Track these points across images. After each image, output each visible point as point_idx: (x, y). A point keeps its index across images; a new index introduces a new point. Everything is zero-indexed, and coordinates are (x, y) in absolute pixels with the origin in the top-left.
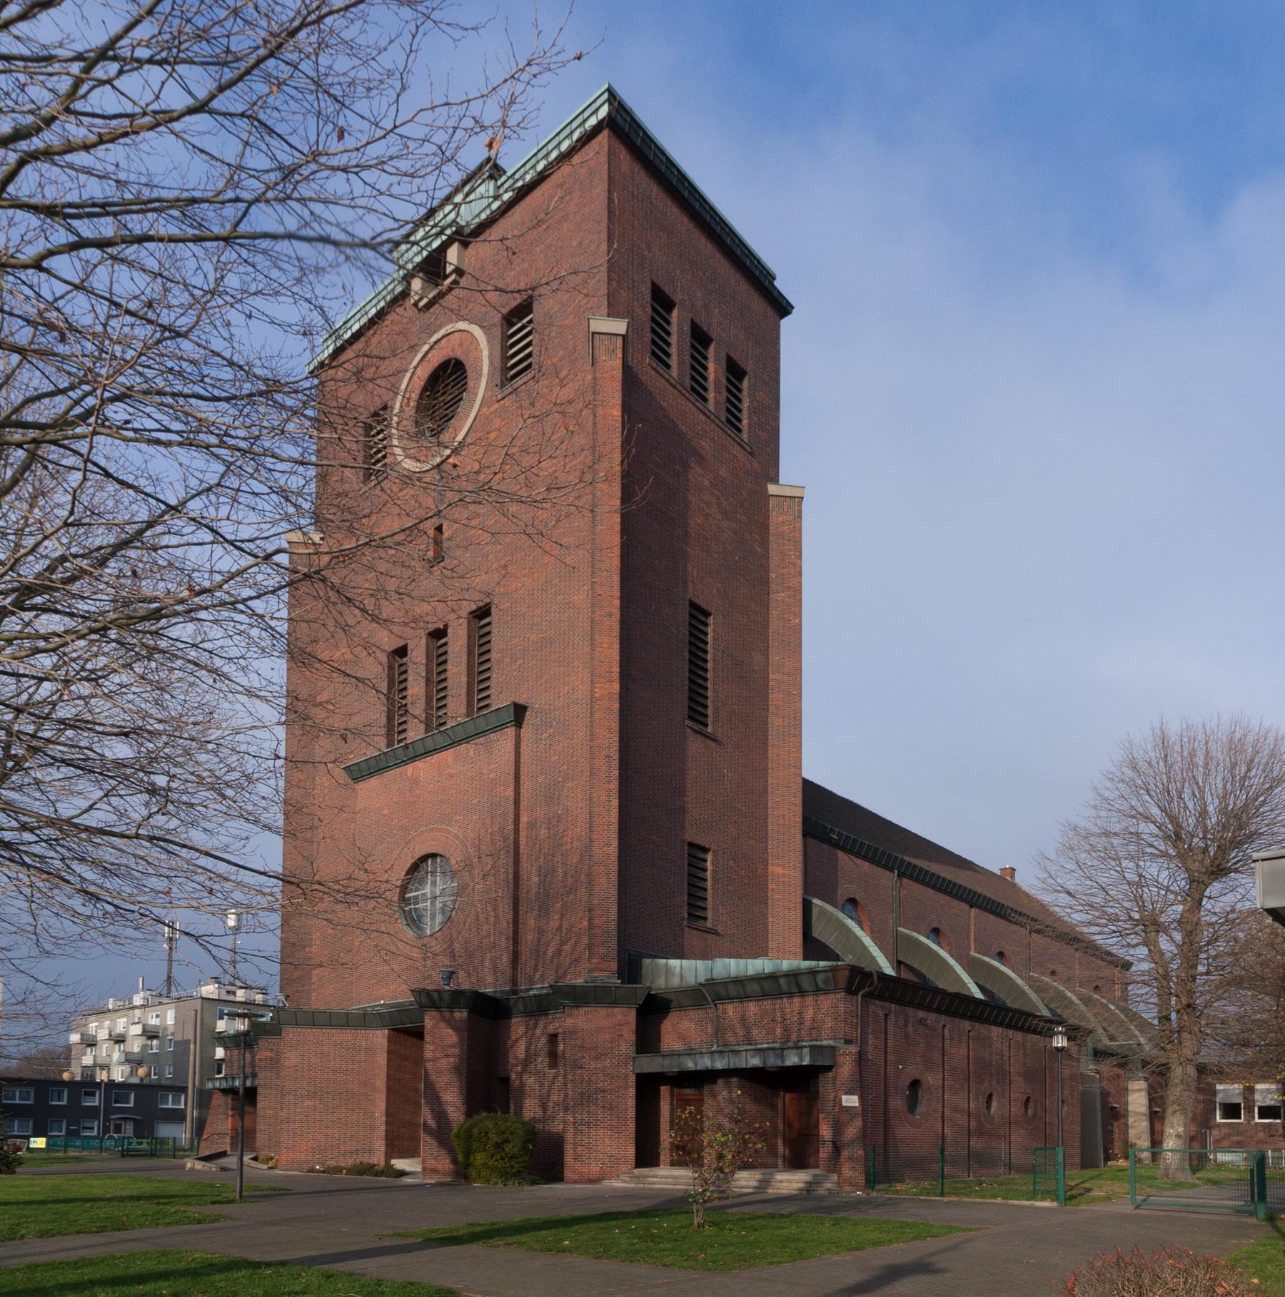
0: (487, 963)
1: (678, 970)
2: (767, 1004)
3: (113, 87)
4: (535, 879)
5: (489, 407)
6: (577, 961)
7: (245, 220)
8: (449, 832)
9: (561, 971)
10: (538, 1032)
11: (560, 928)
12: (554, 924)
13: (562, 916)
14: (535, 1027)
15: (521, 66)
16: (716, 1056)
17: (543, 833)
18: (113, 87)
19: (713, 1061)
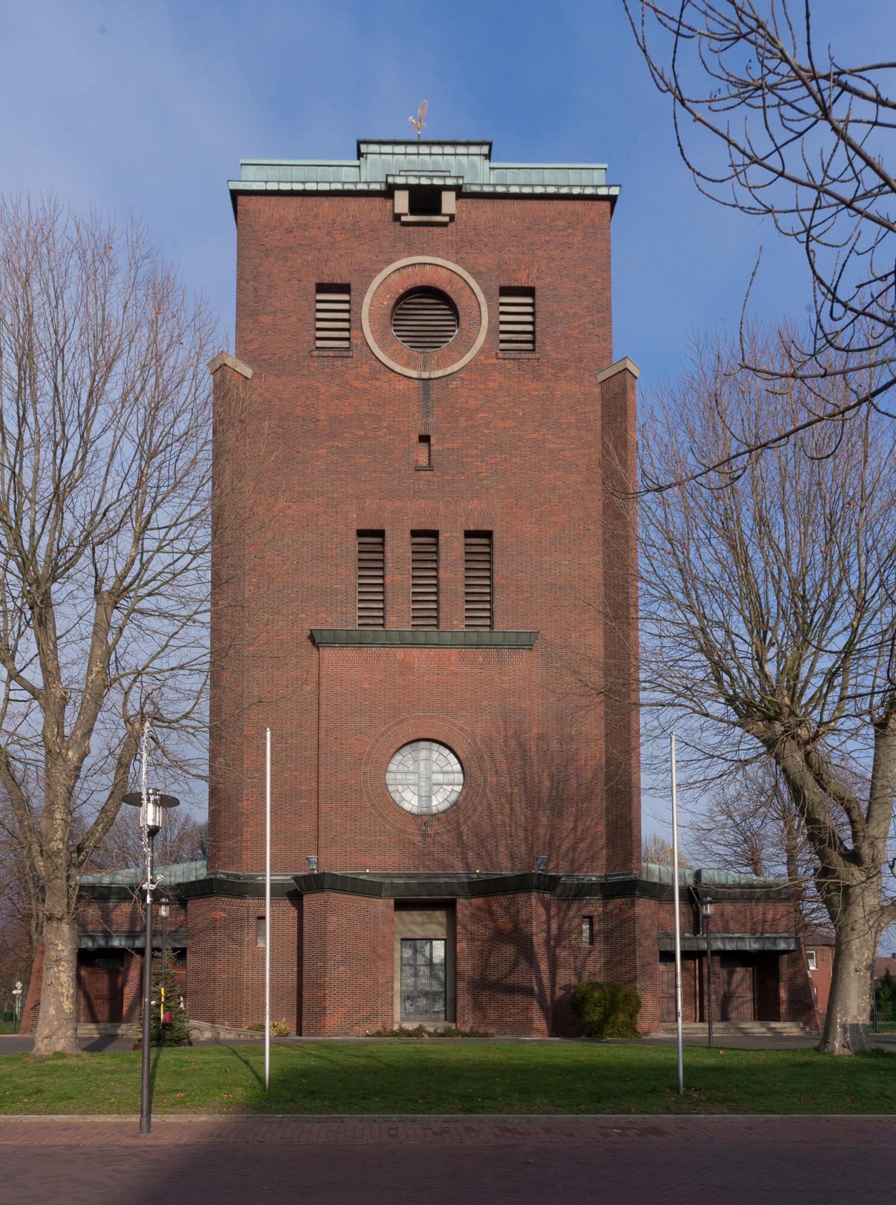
0: (502, 849)
1: (657, 873)
2: (739, 906)
3: (809, 210)
4: (547, 783)
5: (487, 358)
6: (593, 858)
7: (862, 364)
8: (454, 724)
9: (576, 865)
10: (572, 913)
11: (574, 829)
12: (568, 823)
13: (576, 820)
14: (568, 908)
15: (852, 304)
16: (726, 941)
17: (555, 746)
18: (809, 210)
19: (788, 944)
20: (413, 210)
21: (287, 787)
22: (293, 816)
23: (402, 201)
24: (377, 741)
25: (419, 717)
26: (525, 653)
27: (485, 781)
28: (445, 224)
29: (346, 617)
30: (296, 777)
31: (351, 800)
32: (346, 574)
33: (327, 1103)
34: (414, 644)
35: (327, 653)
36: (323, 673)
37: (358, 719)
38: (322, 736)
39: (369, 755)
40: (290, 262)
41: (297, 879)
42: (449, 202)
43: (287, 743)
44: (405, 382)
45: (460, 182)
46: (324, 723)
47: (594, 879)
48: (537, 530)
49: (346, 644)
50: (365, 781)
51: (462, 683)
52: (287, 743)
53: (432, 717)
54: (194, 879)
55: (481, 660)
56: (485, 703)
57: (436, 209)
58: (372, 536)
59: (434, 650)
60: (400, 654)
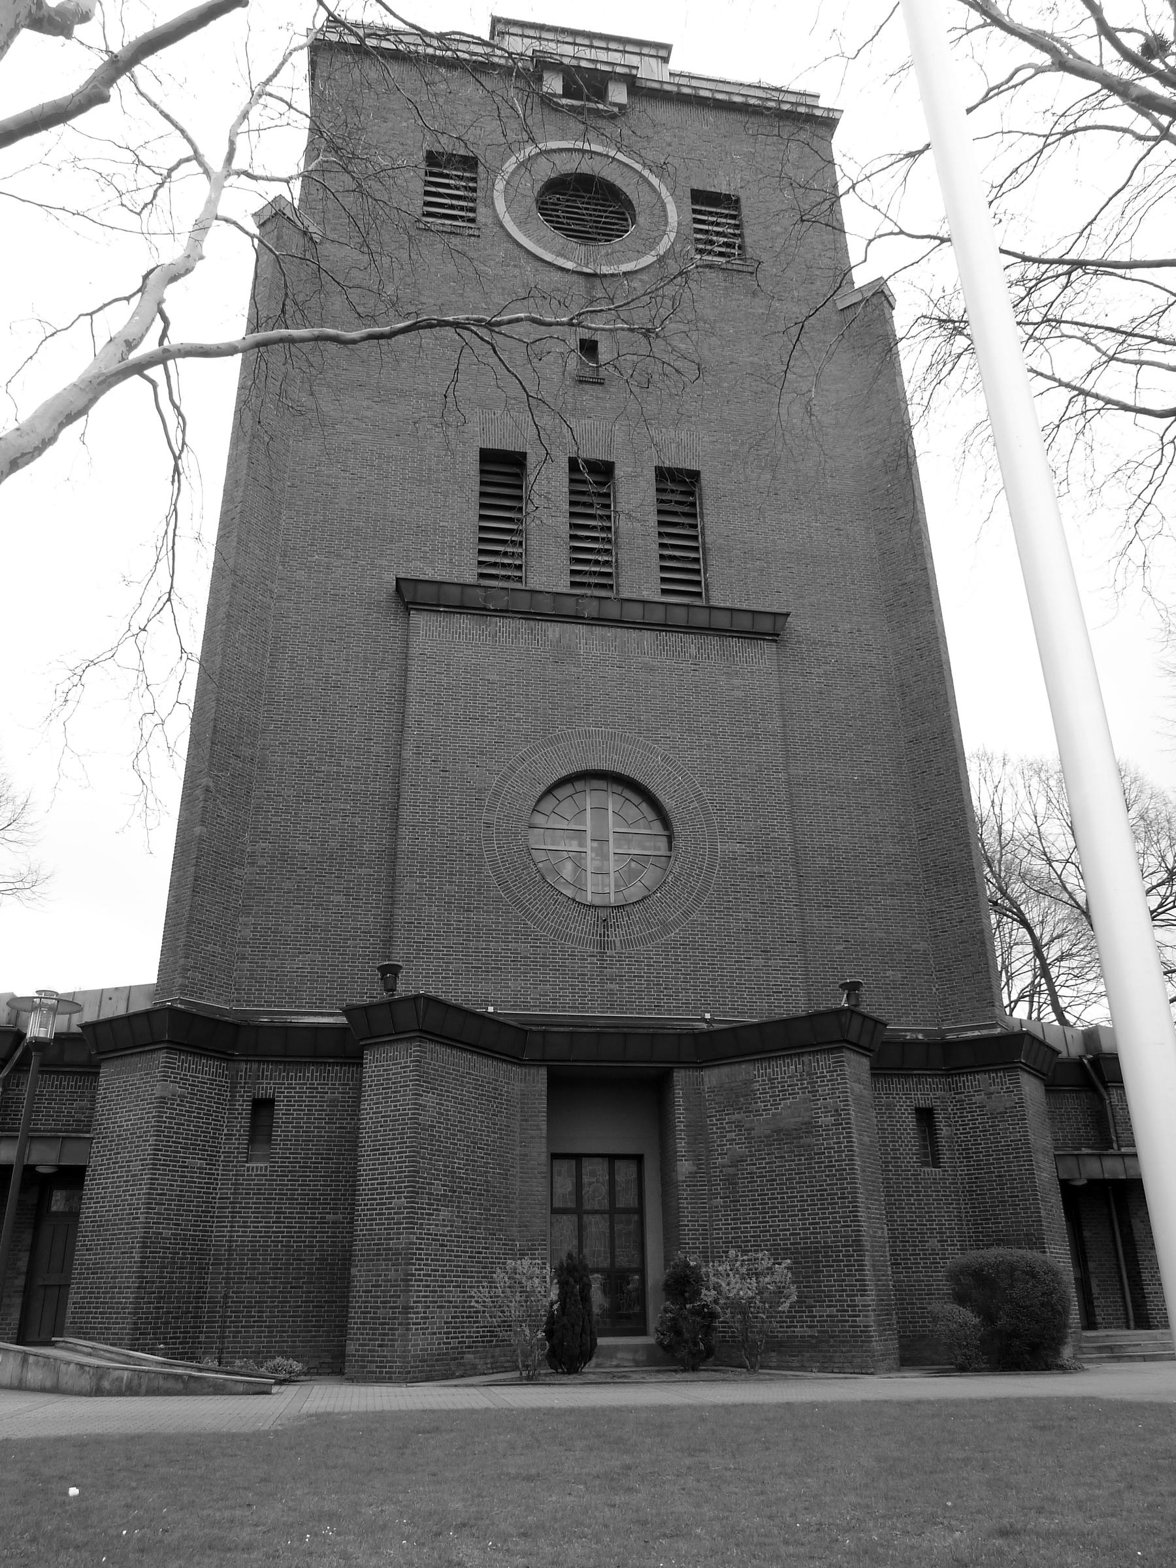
20: (567, 94)
21: (333, 844)
22: (341, 898)
23: (554, 84)
24: (512, 769)
25: (588, 735)
26: (769, 648)
27: (713, 851)
28: (613, 117)
29: (459, 565)
30: (353, 825)
31: (461, 872)
32: (461, 503)
33: (231, 562)
34: (576, 619)
35: (420, 620)
36: (415, 651)
37: (477, 731)
38: (408, 754)
39: (496, 794)
40: (390, 124)
41: (879, 297)
42: (618, 94)
43: (339, 765)
44: (557, 276)
45: (634, 72)
46: (412, 734)
47: (920, 1037)
48: (769, 476)
49: (462, 608)
50: (489, 839)
51: (663, 685)
52: (339, 765)
53: (613, 736)
54: (121, 1011)
55: (693, 651)
56: (704, 719)
57: (601, 95)
58: (503, 470)
59: (613, 630)
60: (554, 631)
